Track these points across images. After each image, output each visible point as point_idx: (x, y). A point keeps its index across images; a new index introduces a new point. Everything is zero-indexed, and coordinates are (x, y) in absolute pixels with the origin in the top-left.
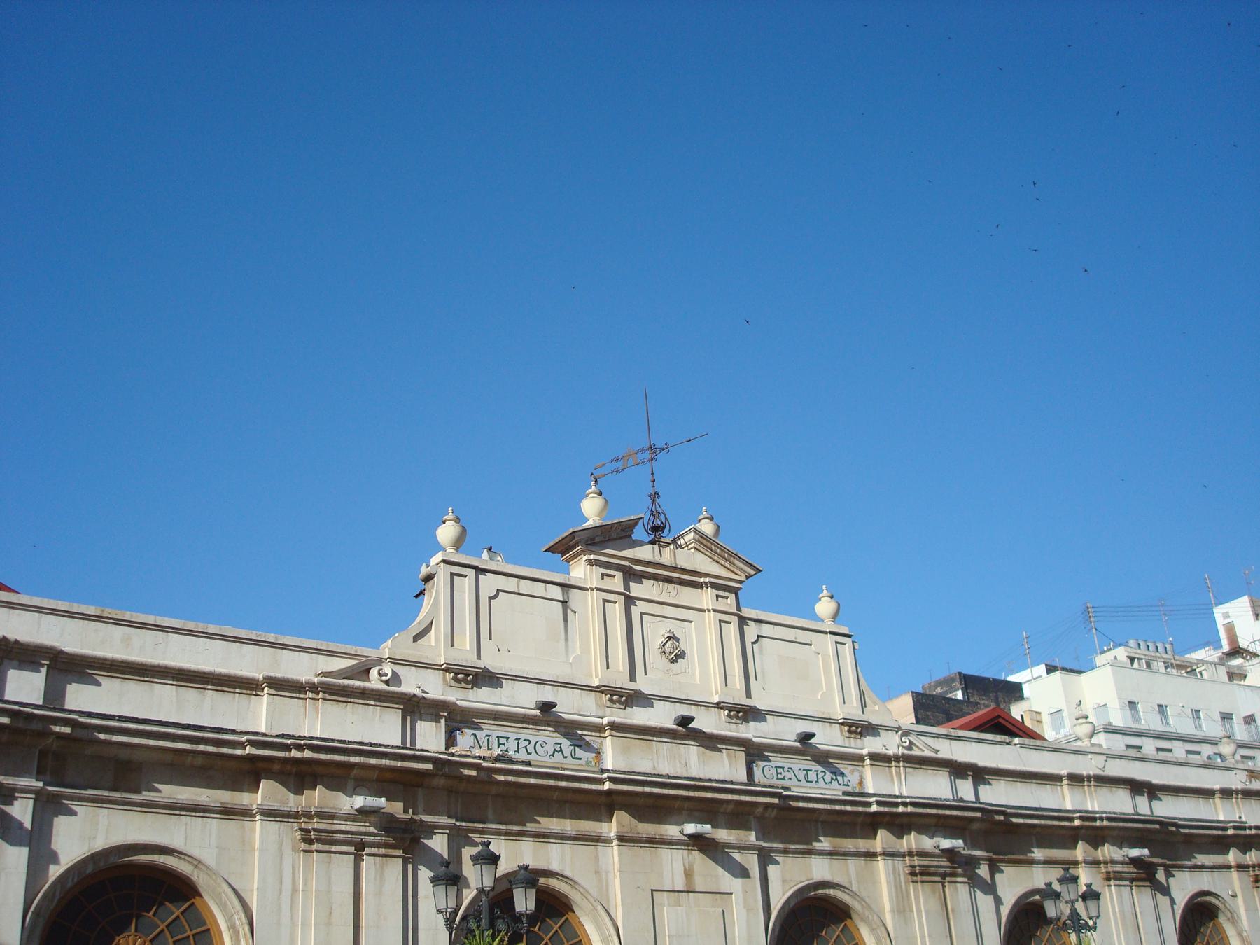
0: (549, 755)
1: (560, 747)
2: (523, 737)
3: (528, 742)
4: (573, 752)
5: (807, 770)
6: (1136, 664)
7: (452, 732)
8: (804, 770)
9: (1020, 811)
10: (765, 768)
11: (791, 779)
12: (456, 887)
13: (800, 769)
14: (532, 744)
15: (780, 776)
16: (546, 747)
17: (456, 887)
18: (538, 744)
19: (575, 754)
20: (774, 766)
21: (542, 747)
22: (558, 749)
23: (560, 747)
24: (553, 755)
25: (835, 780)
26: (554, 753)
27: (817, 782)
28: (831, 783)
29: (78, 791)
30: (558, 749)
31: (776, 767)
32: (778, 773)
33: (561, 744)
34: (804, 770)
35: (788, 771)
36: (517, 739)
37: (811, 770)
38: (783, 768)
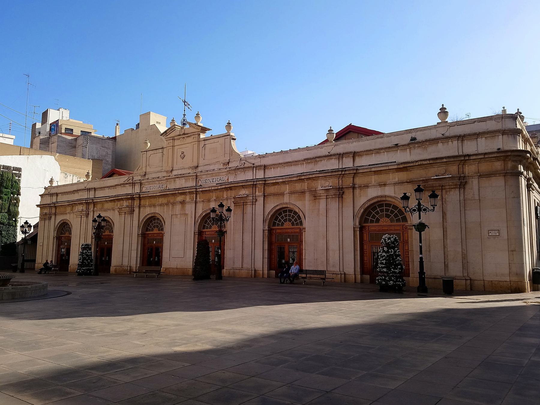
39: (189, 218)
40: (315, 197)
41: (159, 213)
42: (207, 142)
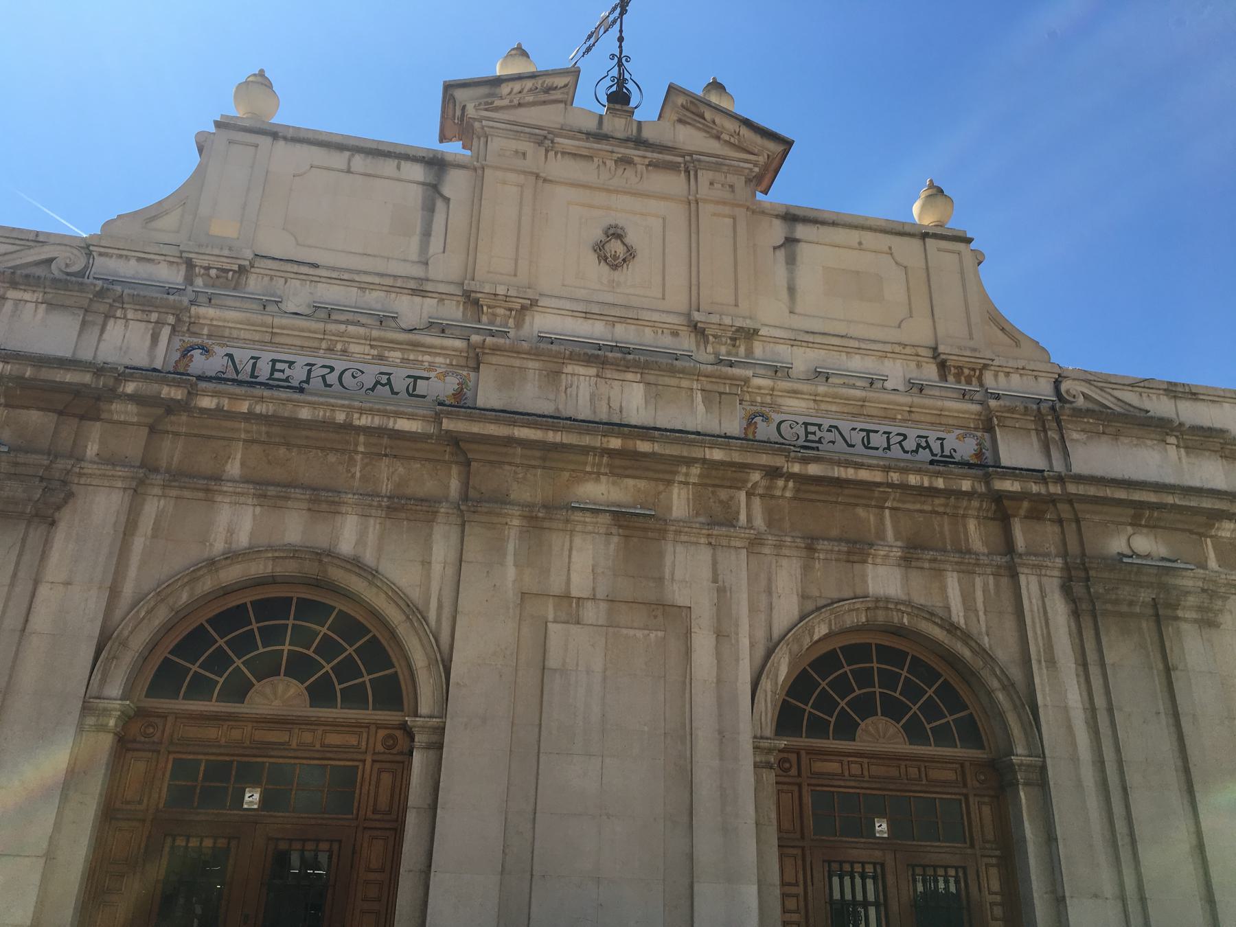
0: (364, 389)
1: (927, 442)
2: (895, 430)
3: (902, 438)
4: (865, 439)
5: (868, 432)
6: (779, 374)
7: (753, 419)
8: (861, 430)
9: (1109, 492)
10: (783, 426)
11: (833, 442)
12: (465, 288)
13: (854, 429)
14: (336, 374)
15: (811, 437)
16: (361, 378)
17: (465, 288)
18: (348, 375)
19: (414, 389)
20: (801, 423)
21: (792, 428)
22: (924, 444)
23: (927, 442)
24: (373, 389)
25: (924, 448)
26: (375, 386)
27: (888, 448)
28: (916, 451)
29: (63, 221)
30: (924, 444)
31: (806, 424)
32: (807, 433)
33: (390, 374)
34: (861, 430)
35: (829, 431)
36: (938, 439)
37: (877, 432)
38: (820, 426)
39: (703, 643)
42: (801, 231)
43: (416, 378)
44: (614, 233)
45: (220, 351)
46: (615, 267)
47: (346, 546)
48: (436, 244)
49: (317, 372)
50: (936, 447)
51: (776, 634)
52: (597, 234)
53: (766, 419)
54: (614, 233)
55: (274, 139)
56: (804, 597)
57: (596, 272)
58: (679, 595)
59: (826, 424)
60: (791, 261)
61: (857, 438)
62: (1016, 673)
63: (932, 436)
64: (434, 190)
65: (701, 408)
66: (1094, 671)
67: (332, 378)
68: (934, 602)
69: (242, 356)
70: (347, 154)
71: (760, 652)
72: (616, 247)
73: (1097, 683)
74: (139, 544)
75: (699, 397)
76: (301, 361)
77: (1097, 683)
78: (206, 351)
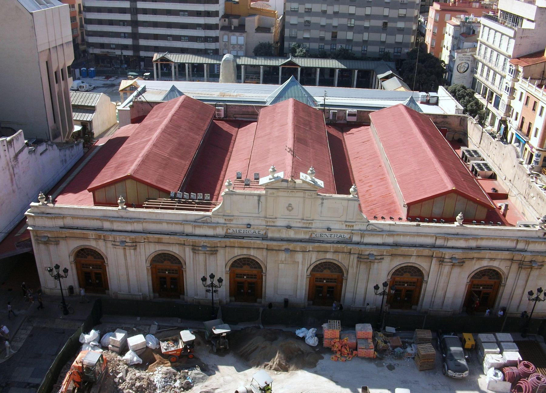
40: (441, 261)
41: (255, 255)
43: (259, 231)
44: (290, 205)
45: (232, 229)
46: (290, 211)
47: (252, 254)
48: (260, 210)
49: (245, 231)
50: (343, 236)
51: (312, 263)
52: (287, 205)
53: (314, 234)
54: (290, 205)
55: (298, 18)
56: (316, 258)
57: (287, 212)
58: (297, 260)
59: (324, 234)
60: (322, 206)
61: (329, 236)
62: (347, 267)
63: (342, 235)
64: (259, 200)
65: (303, 234)
66: (358, 268)
67: (247, 232)
68: (337, 259)
69: (234, 230)
70: (244, 196)
71: (309, 265)
72: (290, 208)
73: (356, 286)
74: (227, 254)
75: (303, 233)
76: (243, 230)
77: (356, 286)
78: (229, 229)
